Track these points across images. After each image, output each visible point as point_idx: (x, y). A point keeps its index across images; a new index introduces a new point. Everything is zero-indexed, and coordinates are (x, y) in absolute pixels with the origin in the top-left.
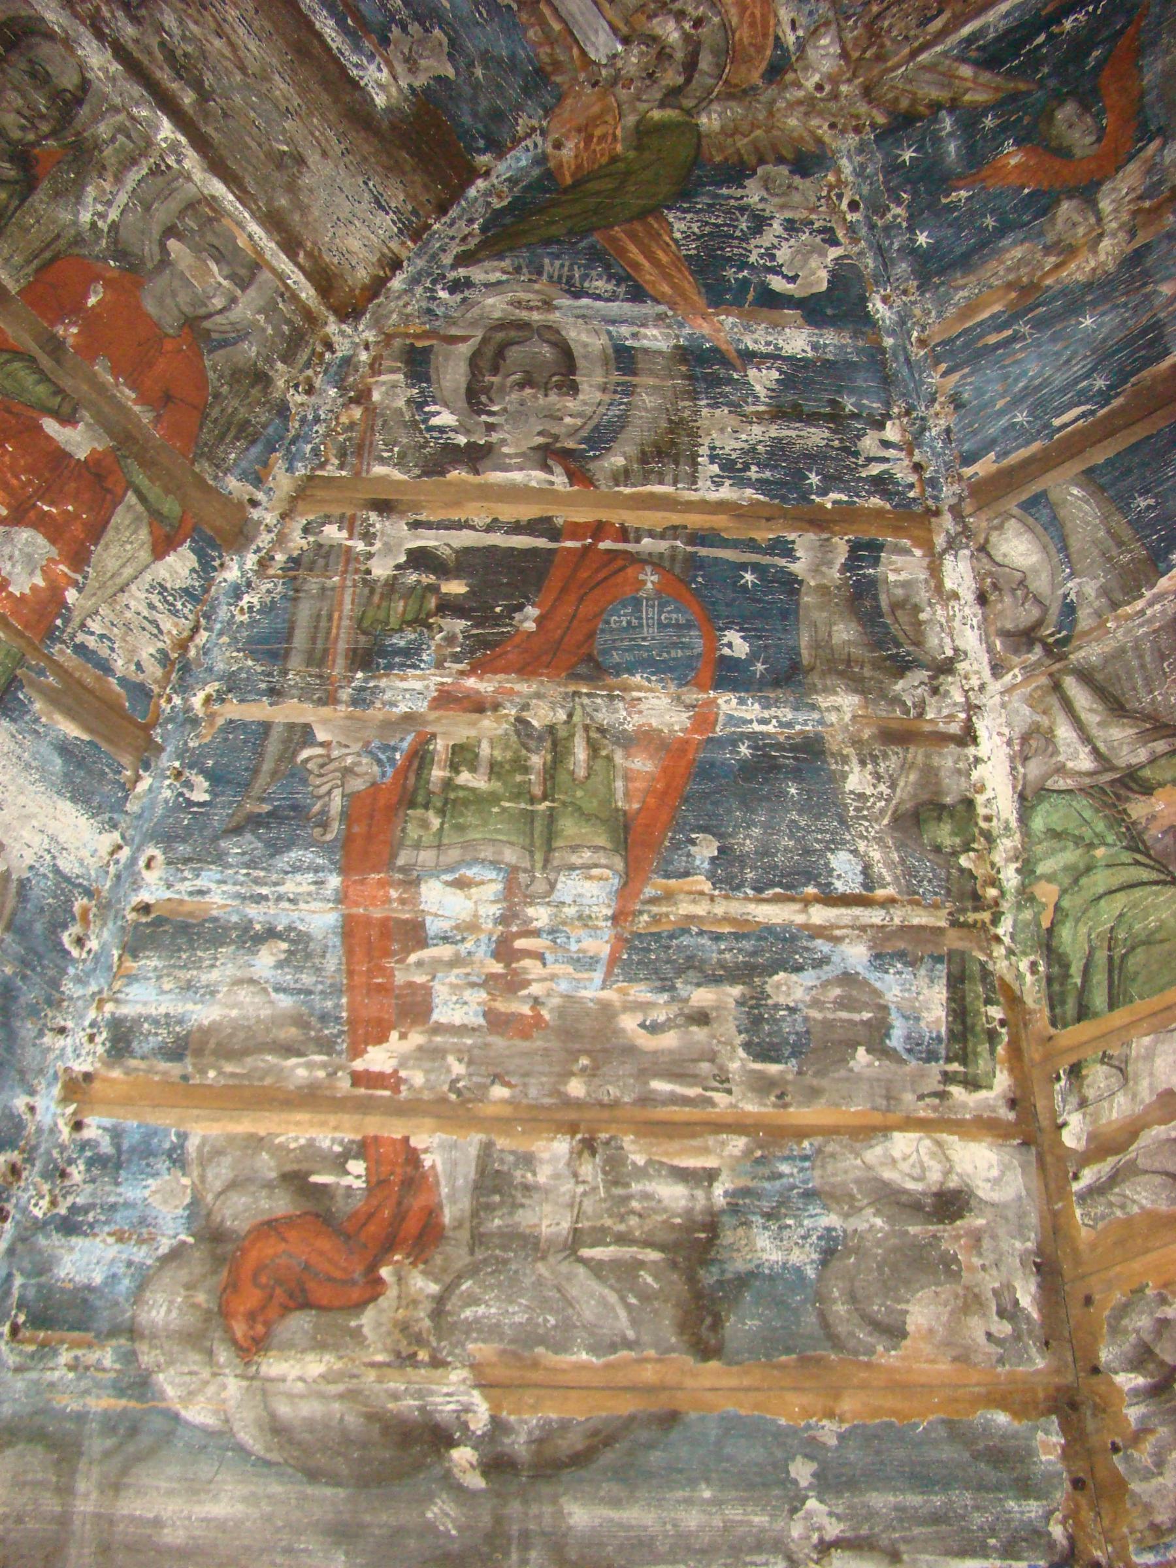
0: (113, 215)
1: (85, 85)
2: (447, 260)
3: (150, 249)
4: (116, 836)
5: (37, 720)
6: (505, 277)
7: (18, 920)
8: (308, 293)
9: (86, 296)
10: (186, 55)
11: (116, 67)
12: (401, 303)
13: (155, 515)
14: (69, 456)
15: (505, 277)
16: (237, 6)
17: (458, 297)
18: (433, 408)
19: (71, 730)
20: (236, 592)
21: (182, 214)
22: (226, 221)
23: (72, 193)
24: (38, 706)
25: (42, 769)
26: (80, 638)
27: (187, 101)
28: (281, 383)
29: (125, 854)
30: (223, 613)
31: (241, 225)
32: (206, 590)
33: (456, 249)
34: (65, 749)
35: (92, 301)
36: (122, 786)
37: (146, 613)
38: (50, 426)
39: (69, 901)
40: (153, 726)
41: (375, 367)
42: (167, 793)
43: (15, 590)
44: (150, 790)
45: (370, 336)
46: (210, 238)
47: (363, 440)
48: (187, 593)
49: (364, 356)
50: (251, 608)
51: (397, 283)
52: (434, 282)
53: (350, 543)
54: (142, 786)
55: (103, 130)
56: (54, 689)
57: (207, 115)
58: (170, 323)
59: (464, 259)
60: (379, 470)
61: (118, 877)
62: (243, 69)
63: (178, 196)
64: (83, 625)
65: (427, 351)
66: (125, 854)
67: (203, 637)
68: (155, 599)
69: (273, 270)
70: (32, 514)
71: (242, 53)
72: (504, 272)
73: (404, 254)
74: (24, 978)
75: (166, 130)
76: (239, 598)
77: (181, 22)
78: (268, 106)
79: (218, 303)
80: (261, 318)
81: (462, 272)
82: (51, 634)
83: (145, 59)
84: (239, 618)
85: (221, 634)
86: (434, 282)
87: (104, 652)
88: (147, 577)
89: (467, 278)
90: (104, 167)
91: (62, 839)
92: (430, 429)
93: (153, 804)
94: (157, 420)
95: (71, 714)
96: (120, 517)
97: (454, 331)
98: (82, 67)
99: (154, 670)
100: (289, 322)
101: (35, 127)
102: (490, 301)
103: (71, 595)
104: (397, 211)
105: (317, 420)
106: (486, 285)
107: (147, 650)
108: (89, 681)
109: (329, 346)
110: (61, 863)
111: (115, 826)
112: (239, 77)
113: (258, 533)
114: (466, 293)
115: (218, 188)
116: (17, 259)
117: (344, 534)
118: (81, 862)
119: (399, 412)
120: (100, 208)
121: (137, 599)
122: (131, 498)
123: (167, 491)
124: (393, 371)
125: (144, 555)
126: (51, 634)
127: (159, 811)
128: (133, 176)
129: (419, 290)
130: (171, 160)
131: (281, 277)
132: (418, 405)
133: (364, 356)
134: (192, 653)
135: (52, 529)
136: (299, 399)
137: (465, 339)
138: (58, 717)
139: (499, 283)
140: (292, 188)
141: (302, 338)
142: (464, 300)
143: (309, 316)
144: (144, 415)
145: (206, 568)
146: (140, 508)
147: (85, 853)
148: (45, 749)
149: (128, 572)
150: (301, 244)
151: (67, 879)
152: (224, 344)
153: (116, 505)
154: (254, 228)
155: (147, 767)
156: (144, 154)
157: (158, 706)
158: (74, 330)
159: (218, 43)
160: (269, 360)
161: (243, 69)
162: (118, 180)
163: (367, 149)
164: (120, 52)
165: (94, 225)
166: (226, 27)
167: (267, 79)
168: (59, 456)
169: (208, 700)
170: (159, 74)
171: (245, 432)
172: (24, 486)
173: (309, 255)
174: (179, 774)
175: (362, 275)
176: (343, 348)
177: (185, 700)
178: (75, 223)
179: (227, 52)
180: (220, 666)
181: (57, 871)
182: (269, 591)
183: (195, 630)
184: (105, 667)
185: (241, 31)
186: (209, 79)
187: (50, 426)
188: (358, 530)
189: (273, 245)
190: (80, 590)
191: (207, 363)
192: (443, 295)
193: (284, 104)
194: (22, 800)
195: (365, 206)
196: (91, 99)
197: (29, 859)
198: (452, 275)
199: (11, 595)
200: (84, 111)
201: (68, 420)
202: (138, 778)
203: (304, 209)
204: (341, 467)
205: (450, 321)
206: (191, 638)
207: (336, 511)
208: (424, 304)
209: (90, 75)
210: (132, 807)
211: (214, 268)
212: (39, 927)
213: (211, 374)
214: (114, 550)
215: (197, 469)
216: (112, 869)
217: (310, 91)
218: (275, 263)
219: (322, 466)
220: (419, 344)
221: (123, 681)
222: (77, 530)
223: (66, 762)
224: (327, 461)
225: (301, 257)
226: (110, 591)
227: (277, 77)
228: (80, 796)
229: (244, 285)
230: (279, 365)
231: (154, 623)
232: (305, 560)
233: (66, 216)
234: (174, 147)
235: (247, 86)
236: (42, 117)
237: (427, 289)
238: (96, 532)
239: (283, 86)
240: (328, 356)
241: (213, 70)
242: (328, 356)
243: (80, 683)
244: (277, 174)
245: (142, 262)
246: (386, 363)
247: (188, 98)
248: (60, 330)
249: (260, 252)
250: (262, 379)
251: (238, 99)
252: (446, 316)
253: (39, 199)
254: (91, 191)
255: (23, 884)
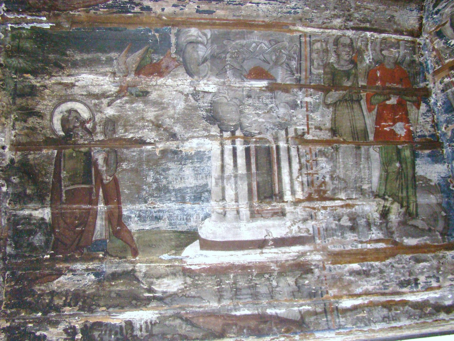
0: (371, 57)
1: (351, 39)
2: (431, 9)
3: (381, 57)
4: (447, 164)
5: (421, 155)
6: (446, 3)
7: (442, 190)
8: (410, 38)
9: (377, 75)
10: (363, 18)
11: (354, 32)
12: (427, 24)
13: (414, 102)
14: (394, 105)
15: (446, 3)
16: (365, 2)
17: (439, 15)
18: (449, 42)
19: (427, 152)
20: (435, 104)
21: (381, 46)
22: (388, 40)
23: (363, 60)
24: (420, 152)
25: (428, 162)
26: (418, 134)
27: (368, 26)
28: (417, 59)
29: (450, 165)
30: (436, 109)
31: (391, 38)
32: (430, 108)
33: (431, 5)
34: (429, 156)
35: (378, 75)
36: (441, 154)
37: (424, 121)
38: (388, 102)
39: (447, 181)
40: (438, 140)
41: (432, 42)
42: (450, 150)
43: (403, 135)
44: (446, 151)
45: (426, 36)
46: (388, 45)
47: (439, 58)
48: (428, 111)
49: (428, 41)
50: (441, 105)
51: (424, 22)
52: (431, 15)
53: (451, 80)
54: (445, 152)
55: (359, 44)
56: (420, 147)
57: (373, 25)
58: (392, 66)
59: (434, 7)
60: (447, 61)
61: (452, 171)
62: (373, 11)
63: (378, 43)
64: (417, 132)
65: (440, 31)
66: (450, 165)
67: (435, 116)
68: (424, 117)
69: (402, 40)
70: (396, 120)
71: (371, 8)
72: (445, 2)
73: (422, 15)
74: (449, 199)
75: (368, 34)
76: (437, 104)
77: (358, 13)
78: (382, 13)
79: (397, 55)
80: (406, 51)
81: (436, 9)
82: (413, 138)
83: (357, 26)
84: (439, 108)
85: (438, 114)
86: (431, 15)
87: (423, 134)
88: (420, 114)
89: (438, 9)
90: (364, 50)
91: (439, 171)
92: (452, 46)
93: (448, 154)
94: (402, 85)
95: (426, 149)
96: (409, 108)
97: (443, 23)
98: (349, 37)
99: (432, 130)
100: (410, 47)
101: (350, 55)
102: (446, 10)
103: (411, 128)
104: (416, 8)
105: (427, 60)
106: (443, 8)
107: (429, 127)
108: (424, 141)
109: (419, 44)
110: (442, 176)
111: (445, 162)
112: (373, 13)
113: (431, 90)
114: (440, 13)
115: (383, 35)
116: (363, 79)
117: (449, 79)
118: (444, 173)
119: (443, 47)
120: (368, 58)
121: (421, 120)
122: (408, 103)
123: (412, 96)
124: (436, 39)
125: (417, 111)
126: (413, 138)
127: (450, 154)
128: (369, 47)
129: (429, 19)
130: (373, 38)
131: (403, 40)
132: (446, 43)
133: (428, 41)
134: (436, 121)
135: (400, 120)
136: (422, 59)
137: (446, 23)
138: (424, 151)
139: (446, 6)
140: (395, 23)
141: (414, 47)
142: (440, 14)
143: (413, 42)
144: (399, 86)
145: (427, 104)
146: (410, 103)
147: (444, 171)
148: (426, 158)
149: (416, 116)
150: (403, 31)
151: (444, 178)
152: (403, 62)
153: (406, 106)
154: (394, 36)
155: (443, 148)
156: (368, 41)
157: (437, 136)
158: (379, 82)
159: (366, 11)
160: (412, 57)
161: (373, 11)
162: (367, 50)
163: (403, 3)
164: (353, 29)
165: (370, 62)
166: (366, 7)
167: (378, 9)
168: (393, 106)
169: (445, 128)
170: (361, 26)
171: (418, 74)
172: (391, 116)
173: (406, 32)
174: (449, 145)
175: (417, 26)
176: (422, 42)
177: (441, 131)
178: (367, 64)
179: (369, 11)
180: (442, 120)
181: (442, 177)
182: (442, 100)
183: (433, 117)
184: (424, 136)
185: (368, 5)
186: (369, 18)
187: (388, 102)
188: (451, 77)
189: (399, 36)
190: (412, 126)
191: (403, 68)
192: (435, 16)
193: (383, 10)
194: (429, 170)
195: (409, 13)
196: (354, 41)
197: (437, 179)
198: (434, 11)
199: (403, 137)
200: (354, 44)
201: (389, 99)
202: (443, 151)
203: (399, 25)
204: (439, 66)
205: (441, 21)
206: (434, 119)
207: (444, 75)
208: (432, 21)
209: (351, 37)
210: (445, 157)
211: (392, 50)
212: (446, 189)
213: (405, 69)
214: (412, 114)
215: (414, 87)
216: (450, 170)
217: (386, 3)
218: (401, 39)
219: (435, 68)
220: (438, 30)
221: (429, 136)
222: (404, 116)
223: (431, 158)
224: (435, 67)
225: (405, 33)
226: (416, 122)
227: (379, 7)
228: (436, 162)
229: (398, 48)
230: (414, 56)
231: (426, 121)
232: (444, 89)
233: (365, 65)
234: (372, 36)
235: (376, 13)
236: (349, 52)
237: (431, 18)
238: (407, 114)
239: (381, 7)
240: (421, 46)
241: (369, 16)
242: (421, 46)
243: (423, 142)
244: (391, 23)
245: (381, 60)
246: (433, 39)
247: (368, 25)
248: (377, 84)
249: (397, 40)
250: (413, 62)
251: (376, 17)
252: (439, 21)
253: (359, 66)
254: (365, 56)
255: (439, 184)
